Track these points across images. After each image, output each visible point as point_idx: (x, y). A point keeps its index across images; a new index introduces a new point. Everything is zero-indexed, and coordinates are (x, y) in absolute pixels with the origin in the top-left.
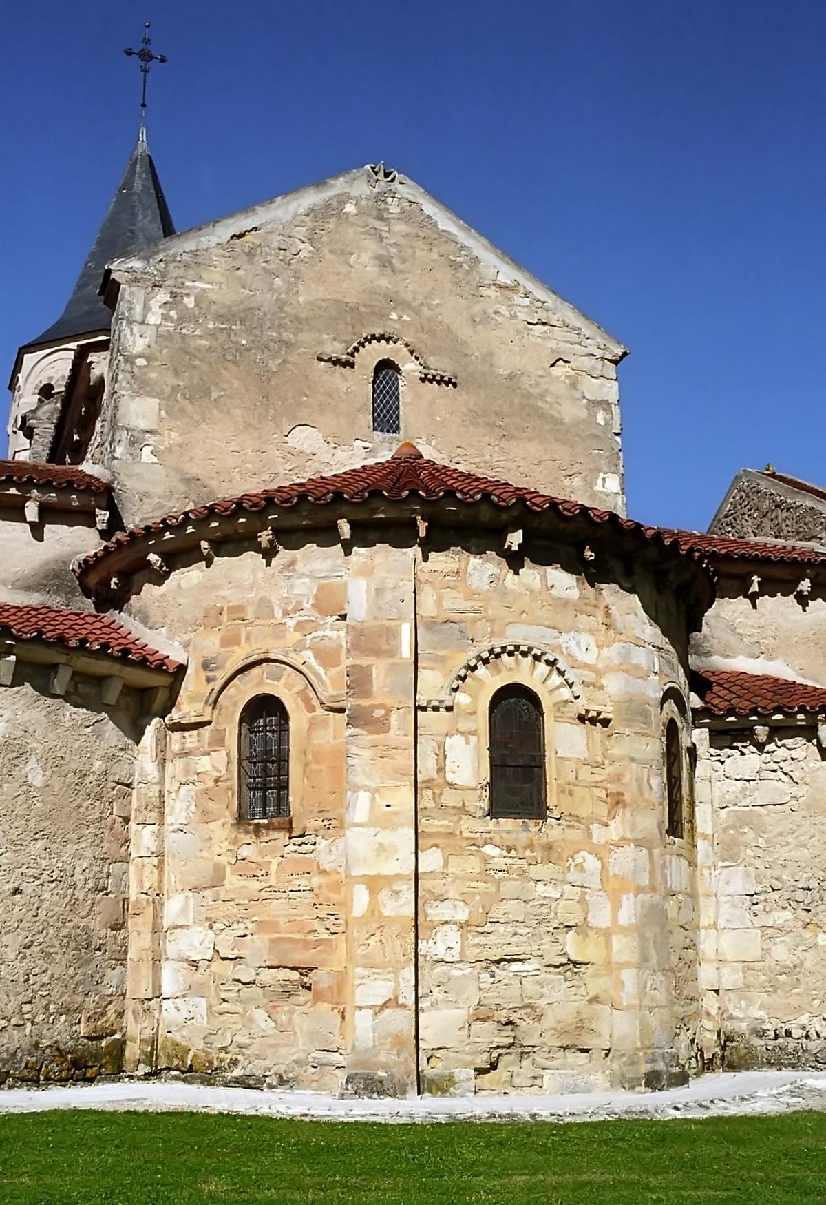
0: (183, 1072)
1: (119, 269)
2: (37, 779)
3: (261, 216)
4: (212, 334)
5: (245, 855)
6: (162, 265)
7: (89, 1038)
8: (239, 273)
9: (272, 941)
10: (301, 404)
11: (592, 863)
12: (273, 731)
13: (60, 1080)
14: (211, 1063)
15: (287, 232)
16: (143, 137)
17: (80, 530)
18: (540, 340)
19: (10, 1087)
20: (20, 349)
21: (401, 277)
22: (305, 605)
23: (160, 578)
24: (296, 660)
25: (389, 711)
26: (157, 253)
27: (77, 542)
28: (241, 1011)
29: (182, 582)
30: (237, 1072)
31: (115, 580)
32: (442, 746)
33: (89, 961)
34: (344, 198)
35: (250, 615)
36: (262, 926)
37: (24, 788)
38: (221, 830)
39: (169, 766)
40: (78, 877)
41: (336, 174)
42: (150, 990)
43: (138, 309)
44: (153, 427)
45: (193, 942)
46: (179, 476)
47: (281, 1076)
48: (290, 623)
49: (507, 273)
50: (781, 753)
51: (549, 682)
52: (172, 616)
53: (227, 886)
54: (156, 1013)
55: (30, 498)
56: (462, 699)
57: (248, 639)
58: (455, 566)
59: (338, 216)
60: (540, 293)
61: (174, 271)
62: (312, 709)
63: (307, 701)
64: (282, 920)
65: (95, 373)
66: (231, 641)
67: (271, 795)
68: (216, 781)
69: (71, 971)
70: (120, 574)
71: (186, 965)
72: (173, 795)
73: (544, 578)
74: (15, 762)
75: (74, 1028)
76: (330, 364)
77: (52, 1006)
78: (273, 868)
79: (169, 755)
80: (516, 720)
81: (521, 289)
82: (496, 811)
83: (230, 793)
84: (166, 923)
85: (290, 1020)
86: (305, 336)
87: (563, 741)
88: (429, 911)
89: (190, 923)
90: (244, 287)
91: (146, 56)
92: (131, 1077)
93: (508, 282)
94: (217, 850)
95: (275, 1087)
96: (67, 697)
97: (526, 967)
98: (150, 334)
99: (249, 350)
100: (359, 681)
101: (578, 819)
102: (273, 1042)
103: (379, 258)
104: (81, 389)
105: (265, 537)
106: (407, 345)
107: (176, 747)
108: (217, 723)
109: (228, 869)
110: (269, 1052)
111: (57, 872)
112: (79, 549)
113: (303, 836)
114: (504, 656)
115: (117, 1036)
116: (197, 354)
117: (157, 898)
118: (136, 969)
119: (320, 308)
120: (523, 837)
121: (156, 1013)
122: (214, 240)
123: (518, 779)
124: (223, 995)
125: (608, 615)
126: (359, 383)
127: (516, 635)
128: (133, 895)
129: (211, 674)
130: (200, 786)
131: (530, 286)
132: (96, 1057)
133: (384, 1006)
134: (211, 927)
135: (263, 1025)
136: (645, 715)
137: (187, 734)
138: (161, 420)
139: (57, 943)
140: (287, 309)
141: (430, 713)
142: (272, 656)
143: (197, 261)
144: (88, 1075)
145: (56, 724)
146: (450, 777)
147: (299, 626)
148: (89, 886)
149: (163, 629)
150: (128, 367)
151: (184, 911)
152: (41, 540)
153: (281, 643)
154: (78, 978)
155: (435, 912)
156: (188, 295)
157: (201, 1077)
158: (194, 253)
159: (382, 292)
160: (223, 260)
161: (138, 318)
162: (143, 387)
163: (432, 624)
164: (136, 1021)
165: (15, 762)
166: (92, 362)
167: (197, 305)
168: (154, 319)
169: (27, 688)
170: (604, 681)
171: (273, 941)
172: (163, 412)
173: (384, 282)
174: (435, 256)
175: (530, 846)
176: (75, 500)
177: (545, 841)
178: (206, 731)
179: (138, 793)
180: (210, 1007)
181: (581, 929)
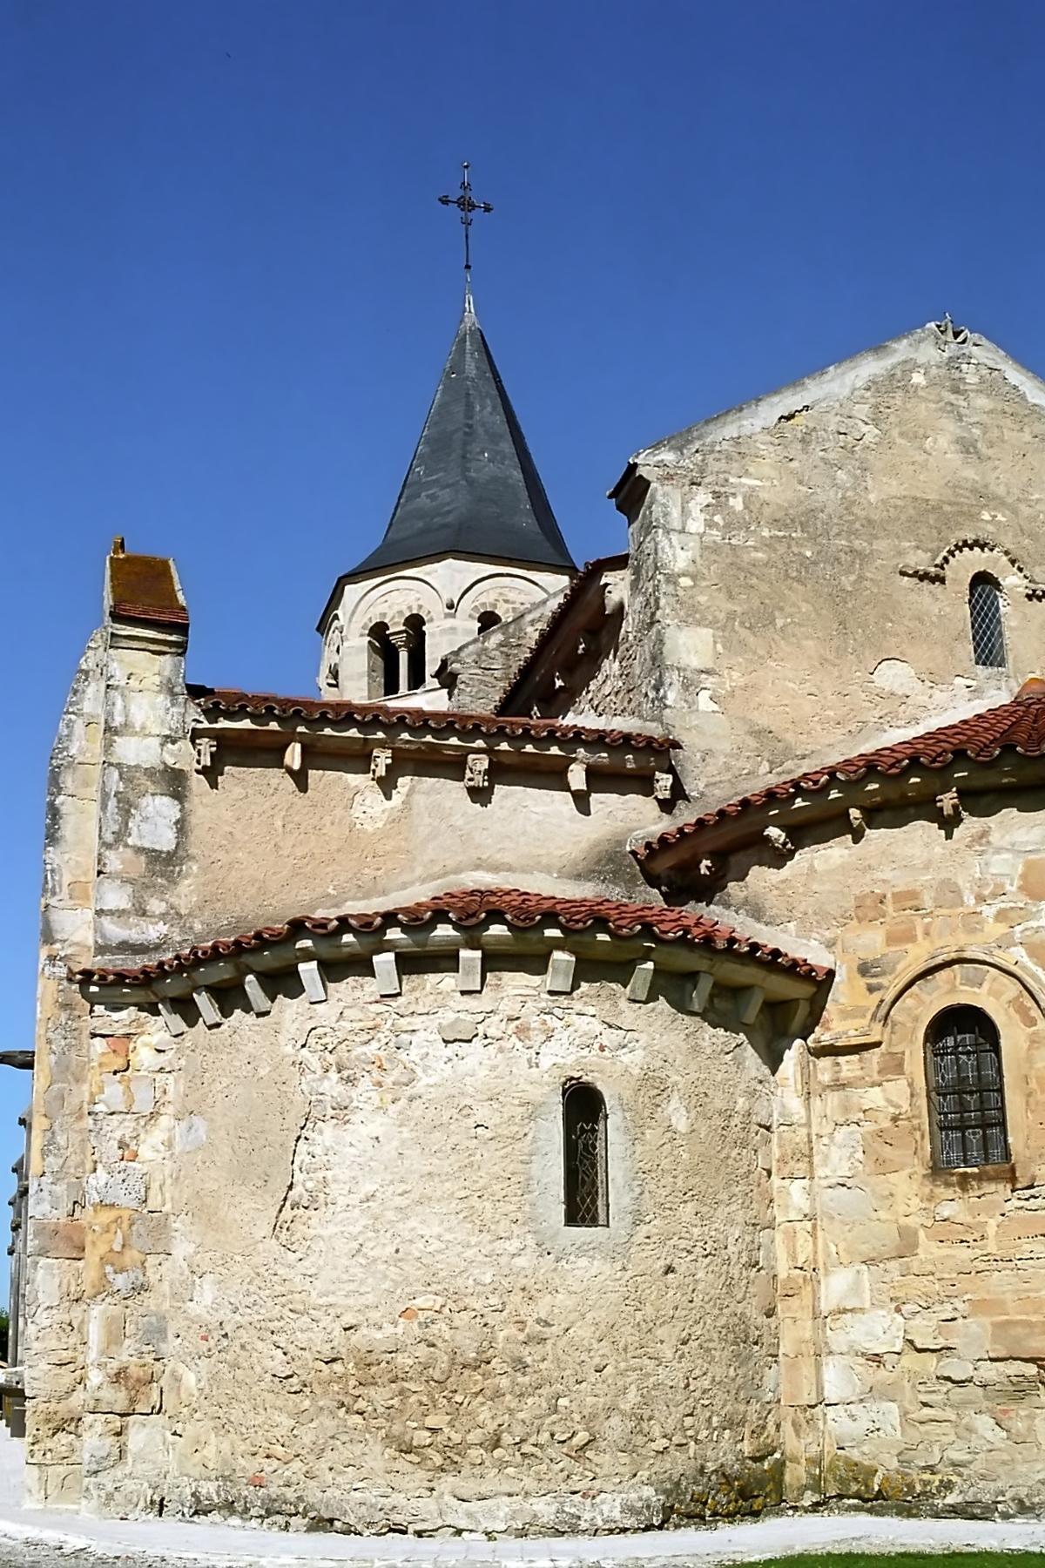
0: (866, 1501)
1: (648, 464)
2: (681, 1124)
3: (813, 391)
4: (768, 545)
5: (946, 1214)
6: (699, 457)
7: (755, 1459)
8: (792, 465)
9: (995, 1325)
10: (884, 632)
12: (968, 1053)
13: (728, 1515)
14: (911, 1486)
15: (846, 412)
16: (470, 306)
17: (634, 799)
19: (677, 1527)
20: (340, 579)
21: (990, 464)
22: (1008, 888)
23: (779, 858)
24: (1006, 958)
26: (691, 442)
27: (633, 818)
28: (953, 1417)
29: (816, 863)
30: (952, 1499)
31: (706, 862)
33: (749, 1358)
34: (908, 367)
35: (928, 901)
36: (979, 1306)
37: (669, 1135)
38: (907, 1185)
39: (816, 1102)
40: (731, 1249)
41: (897, 335)
42: (814, 1394)
43: (675, 513)
44: (710, 665)
45: (879, 1329)
46: (746, 728)
47: (1021, 1502)
48: (988, 911)
52: (794, 905)
53: (922, 1256)
54: (821, 1423)
55: (575, 759)
57: (927, 934)
59: (905, 389)
61: (714, 466)
63: (1023, 1012)
64: (1009, 1297)
65: (612, 599)
67: (974, 1137)
68: (895, 1119)
69: (732, 1373)
70: (711, 855)
71: (862, 1360)
72: (825, 1140)
74: (657, 1101)
75: (739, 1446)
76: (916, 580)
77: (715, 1419)
78: (991, 1230)
79: (814, 1086)
83: (918, 1135)
84: (825, 1307)
85: (1030, 1429)
86: (881, 545)
89: (867, 1305)
90: (800, 483)
91: (466, 205)
92: (795, 1509)
94: (902, 1209)
95: (1013, 1516)
96: (703, 1015)
98: (693, 544)
99: (815, 563)
102: (1006, 1457)
103: (959, 441)
104: (581, 618)
105: (948, 801)
106: (1007, 553)
107: (826, 1078)
108: (890, 1045)
109: (922, 1233)
110: (1001, 1470)
111: (710, 1243)
112: (635, 824)
113: (1031, 1187)
115: (777, 1455)
116: (753, 570)
117: (811, 1272)
118: (793, 1367)
119: (896, 507)
121: (821, 1423)
122: (758, 424)
124: (924, 1398)
126: (953, 604)
128: (783, 1270)
129: (874, 981)
130: (869, 1127)
132: (761, 1484)
134: (898, 1310)
135: (989, 1435)
137: (841, 1059)
138: (718, 656)
139: (715, 1336)
140: (855, 510)
142: (967, 955)
143: (741, 450)
144: (755, 1507)
145: (696, 1050)
147: (1001, 916)
148: (743, 1261)
149: (791, 925)
150: (671, 589)
151: (856, 1288)
152: (588, 814)
153: (979, 938)
154: (739, 1381)
157: (896, 1506)
158: (736, 441)
159: (968, 485)
160: (772, 449)
161: (677, 525)
162: (693, 616)
164: (798, 1435)
165: (657, 1101)
166: (607, 585)
167: (746, 507)
168: (696, 525)
169: (662, 1004)
171: (997, 1326)
172: (719, 646)
173: (970, 473)
174: (1027, 437)
176: (630, 761)
178: (874, 1056)
179: (780, 1138)
180: (905, 1414)
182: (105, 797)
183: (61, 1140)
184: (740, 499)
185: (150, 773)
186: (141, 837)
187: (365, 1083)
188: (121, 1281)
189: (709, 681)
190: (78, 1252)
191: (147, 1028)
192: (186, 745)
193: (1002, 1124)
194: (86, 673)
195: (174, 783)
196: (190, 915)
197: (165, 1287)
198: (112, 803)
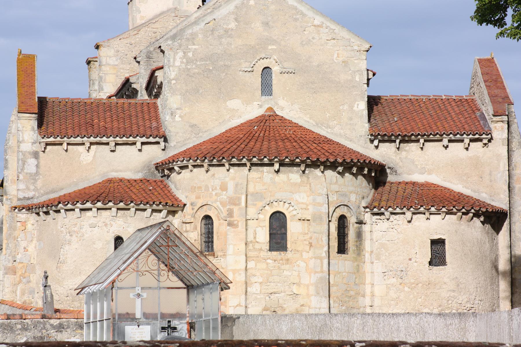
6: (179, 41)
11: (302, 264)
18: (332, 47)
25: (238, 221)
32: (255, 231)
43: (172, 60)
48: (214, 193)
49: (318, 20)
50: (395, 222)
51: (289, 209)
56: (261, 216)
58: (260, 176)
60: (333, 26)
62: (219, 220)
63: (218, 217)
66: (198, 197)
68: (195, 240)
73: (288, 177)
80: (278, 223)
81: (324, 25)
82: (271, 249)
87: (294, 229)
88: (251, 279)
93: (319, 23)
97: (280, 295)
100: (230, 214)
101: (298, 251)
114: (274, 203)
120: (279, 257)
123: (278, 239)
125: (310, 186)
126: (257, 80)
127: (278, 196)
131: (328, 24)
133: (237, 306)
136: (321, 218)
141: (251, 221)
146: (257, 240)
147: (216, 194)
155: (254, 279)
156: (189, 52)
158: (192, 34)
163: (252, 194)
168: (177, 63)
170: (309, 207)
172: (182, 101)
173: (266, 34)
175: (282, 260)
177: (286, 258)
181: (299, 284)
182: (18, 160)
183: (10, 245)
184: (191, 53)
185: (29, 153)
186: (28, 170)
187: (74, 236)
188: (24, 280)
189: (178, 112)
190: (15, 273)
191: (30, 219)
192: (38, 144)
193: (212, 242)
194: (12, 121)
195: (36, 155)
196: (40, 189)
197: (35, 281)
198: (20, 162)
